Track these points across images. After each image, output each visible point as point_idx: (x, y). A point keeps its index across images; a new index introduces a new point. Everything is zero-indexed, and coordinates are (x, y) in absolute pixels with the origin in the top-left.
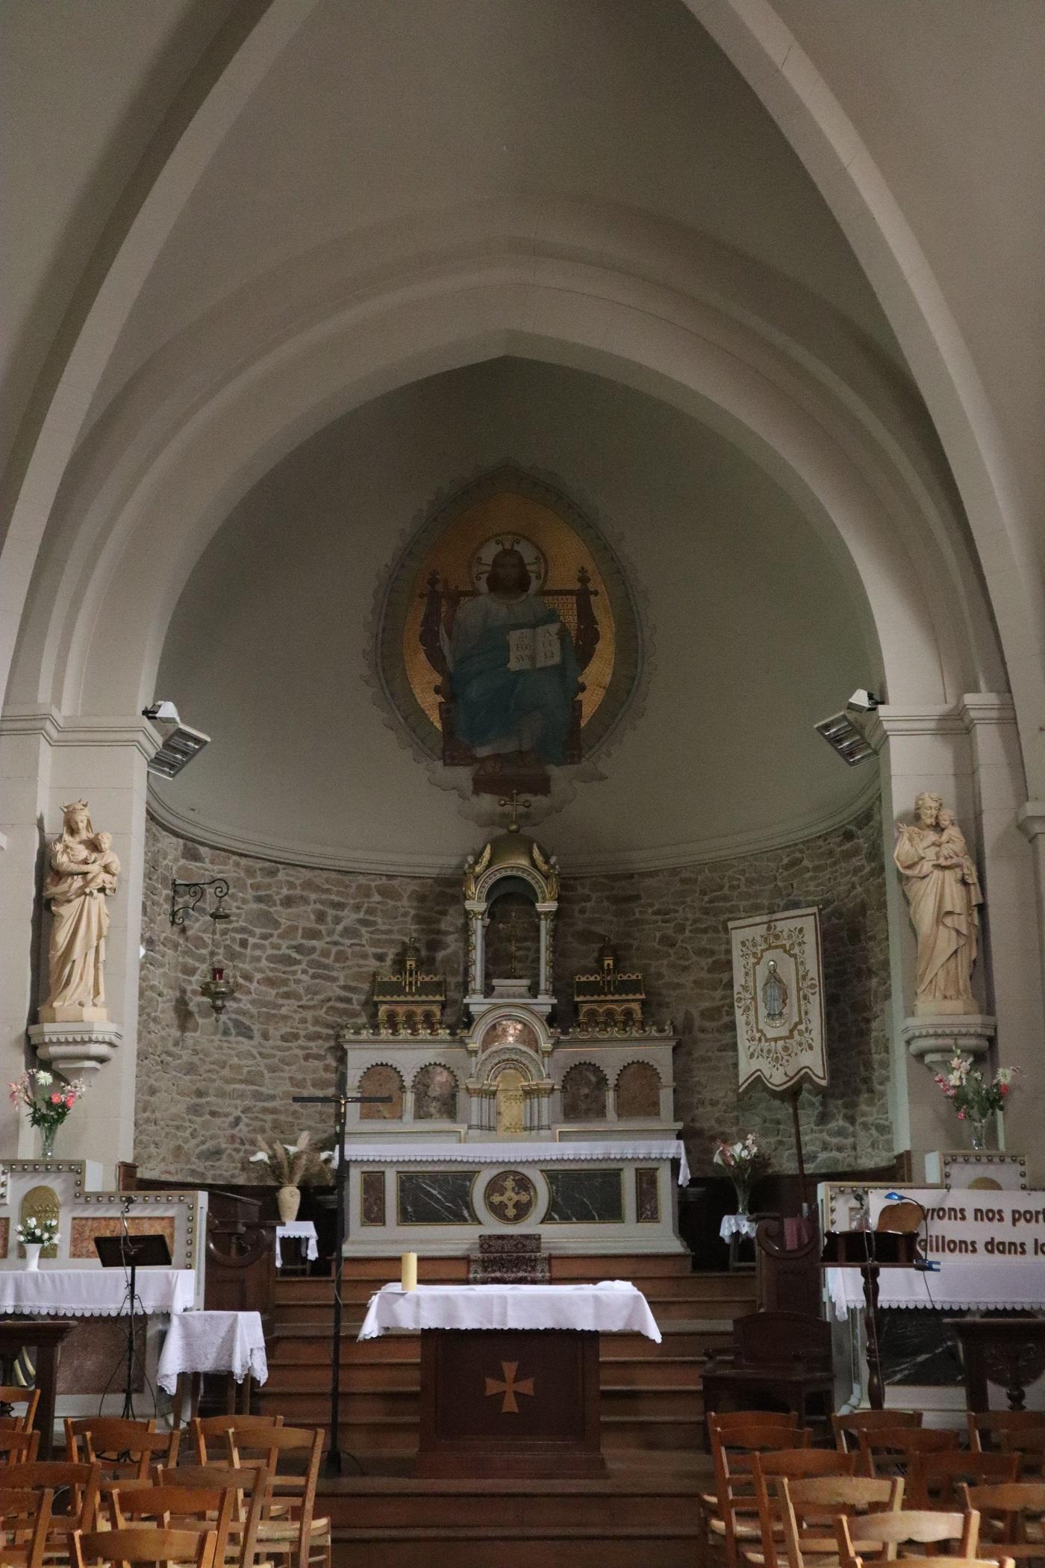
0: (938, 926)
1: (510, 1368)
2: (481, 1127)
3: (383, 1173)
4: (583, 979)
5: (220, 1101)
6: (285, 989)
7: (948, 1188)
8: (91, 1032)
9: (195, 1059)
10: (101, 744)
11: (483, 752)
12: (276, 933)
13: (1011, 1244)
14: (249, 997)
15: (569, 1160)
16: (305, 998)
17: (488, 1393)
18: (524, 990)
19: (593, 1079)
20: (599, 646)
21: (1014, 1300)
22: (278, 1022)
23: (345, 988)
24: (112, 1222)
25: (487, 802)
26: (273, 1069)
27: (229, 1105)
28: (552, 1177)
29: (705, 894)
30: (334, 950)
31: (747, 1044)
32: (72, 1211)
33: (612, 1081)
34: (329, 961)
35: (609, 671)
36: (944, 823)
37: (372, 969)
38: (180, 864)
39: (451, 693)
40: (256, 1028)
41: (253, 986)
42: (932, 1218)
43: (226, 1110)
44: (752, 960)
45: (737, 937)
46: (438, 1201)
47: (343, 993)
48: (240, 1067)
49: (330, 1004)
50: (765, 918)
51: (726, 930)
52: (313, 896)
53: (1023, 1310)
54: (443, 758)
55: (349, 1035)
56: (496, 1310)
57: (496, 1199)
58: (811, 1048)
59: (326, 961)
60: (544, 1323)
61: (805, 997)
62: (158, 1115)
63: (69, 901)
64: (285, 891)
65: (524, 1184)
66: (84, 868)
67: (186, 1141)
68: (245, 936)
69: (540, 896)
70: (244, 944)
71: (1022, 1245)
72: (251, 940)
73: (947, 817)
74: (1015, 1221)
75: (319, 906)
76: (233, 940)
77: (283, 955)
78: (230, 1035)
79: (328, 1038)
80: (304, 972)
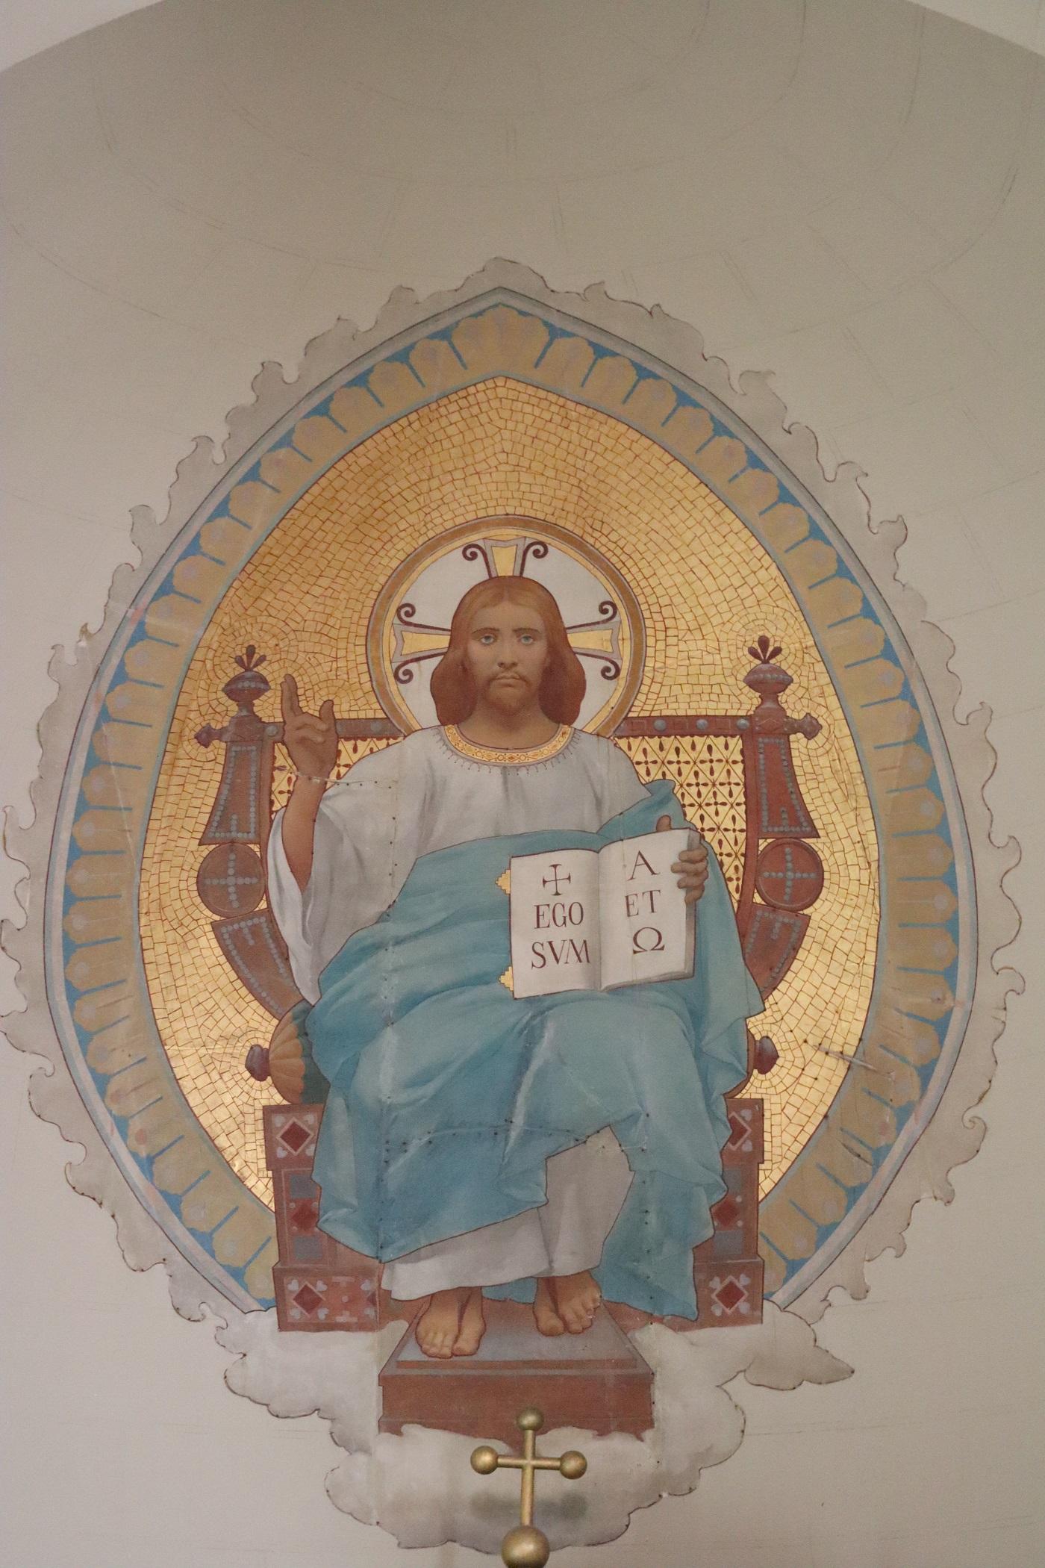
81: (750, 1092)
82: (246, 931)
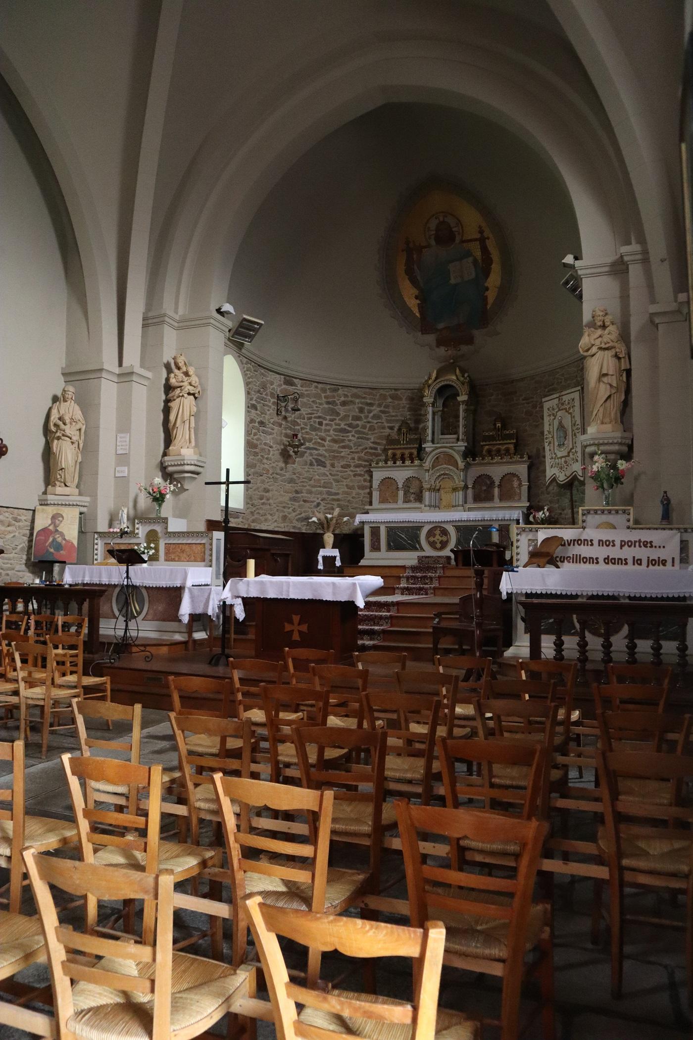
0: (599, 382)
1: (296, 618)
2: (430, 506)
3: (379, 527)
4: (487, 434)
5: (309, 495)
6: (343, 444)
7: (584, 528)
8: (184, 460)
9: (294, 477)
10: (195, 326)
11: (441, 326)
12: (337, 418)
13: (619, 559)
14: (324, 448)
15: (464, 520)
16: (354, 448)
17: (286, 630)
18: (455, 440)
19: (488, 482)
20: (493, 266)
21: (603, 590)
22: (339, 460)
23: (373, 443)
24: (181, 546)
25: (442, 351)
26: (337, 481)
27: (314, 497)
28: (458, 528)
29: (546, 388)
30: (368, 425)
31: (550, 461)
32: (165, 540)
33: (497, 483)
34: (366, 431)
35: (499, 279)
36: (607, 324)
37: (387, 434)
38: (282, 387)
39: (423, 298)
40: (328, 463)
41: (326, 444)
42: (574, 545)
43: (312, 500)
44: (552, 417)
45: (546, 406)
46: (405, 540)
47: (372, 445)
48: (319, 480)
49: (366, 451)
50: (557, 395)
51: (541, 402)
52: (357, 401)
53: (613, 596)
54: (422, 331)
55: (373, 465)
56: (285, 588)
57: (432, 539)
58: (577, 461)
59: (364, 431)
60: (308, 596)
61: (575, 435)
62: (271, 501)
63: (175, 400)
64: (343, 399)
65: (444, 532)
66: (181, 384)
67: (289, 513)
68: (321, 420)
69: (460, 393)
70: (320, 424)
71: (626, 560)
72: (324, 422)
73: (608, 320)
74: (622, 546)
75: (360, 405)
76: (315, 422)
77: (342, 428)
78: (314, 465)
79: (365, 466)
80: (353, 436)
81: (485, 295)
82: (367, 429)
